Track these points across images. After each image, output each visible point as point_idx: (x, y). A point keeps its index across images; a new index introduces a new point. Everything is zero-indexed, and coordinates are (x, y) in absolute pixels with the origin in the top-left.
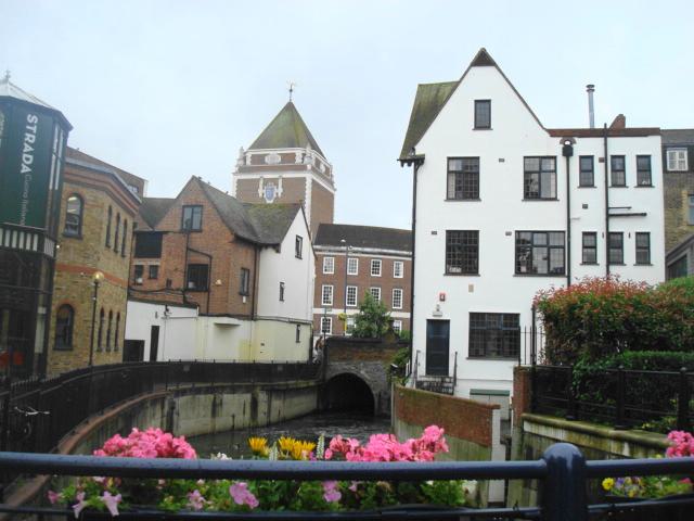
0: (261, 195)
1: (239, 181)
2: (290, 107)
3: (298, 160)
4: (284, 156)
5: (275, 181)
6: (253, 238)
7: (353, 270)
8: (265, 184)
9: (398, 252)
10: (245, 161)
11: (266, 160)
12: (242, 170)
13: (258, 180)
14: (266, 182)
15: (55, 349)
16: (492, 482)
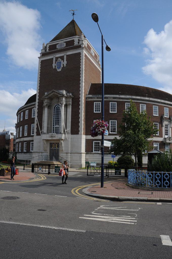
2: (73, 22)
3: (76, 43)
4: (68, 43)
5: (62, 58)
7: (113, 109)
8: (56, 61)
9: (142, 98)
10: (46, 50)
12: (43, 55)
15: (50, 143)
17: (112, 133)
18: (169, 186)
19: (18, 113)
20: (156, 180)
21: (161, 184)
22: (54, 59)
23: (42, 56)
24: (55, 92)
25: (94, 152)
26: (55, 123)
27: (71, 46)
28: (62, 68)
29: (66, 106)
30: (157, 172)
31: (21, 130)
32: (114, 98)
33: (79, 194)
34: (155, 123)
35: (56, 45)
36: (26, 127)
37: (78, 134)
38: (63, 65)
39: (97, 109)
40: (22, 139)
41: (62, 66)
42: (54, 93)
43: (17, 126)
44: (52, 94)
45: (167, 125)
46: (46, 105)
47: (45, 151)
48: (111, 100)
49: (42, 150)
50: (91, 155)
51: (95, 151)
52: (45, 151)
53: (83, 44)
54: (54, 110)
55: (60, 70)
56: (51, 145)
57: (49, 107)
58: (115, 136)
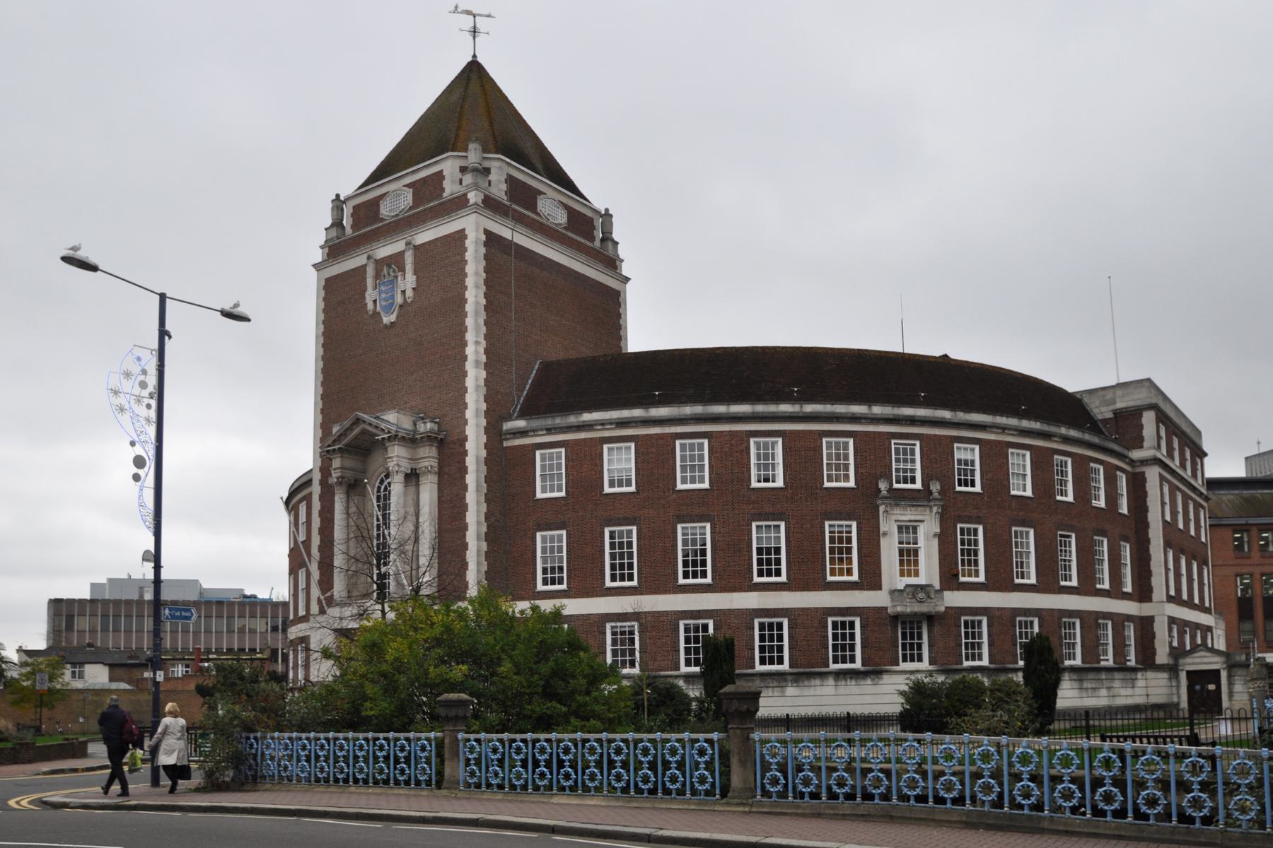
0: (370, 306)
5: (396, 261)
13: (402, 253)
17: (550, 587)
22: (370, 271)
27: (431, 201)
28: (401, 306)
35: (375, 203)
38: (404, 292)
42: (362, 426)
44: (356, 431)
45: (915, 529)
46: (339, 483)
48: (607, 434)
51: (763, 662)
55: (393, 318)
58: (557, 602)
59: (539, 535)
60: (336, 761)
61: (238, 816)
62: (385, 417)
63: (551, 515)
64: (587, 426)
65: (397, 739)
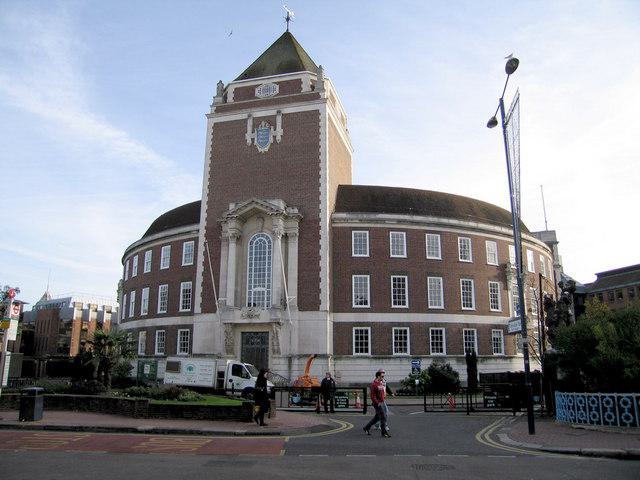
0: (249, 141)
1: (217, 126)
3: (306, 88)
5: (271, 121)
6: (499, 110)
10: (225, 98)
11: (257, 94)
12: (221, 108)
13: (245, 121)
14: (257, 122)
16: (465, 367)
18: (633, 425)
19: (127, 258)
20: (605, 410)
21: (616, 419)
23: (217, 111)
24: (257, 203)
25: (354, 354)
26: (255, 282)
29: (286, 237)
30: (621, 395)
31: (133, 299)
32: (400, 222)
33: (490, 440)
34: (465, 280)
36: (146, 292)
37: (318, 309)
38: (275, 137)
39: (361, 251)
40: (149, 323)
41: (271, 140)
43: (125, 288)
47: (229, 350)
48: (392, 226)
49: (219, 347)
50: (349, 362)
51: (357, 351)
52: (229, 350)
53: (324, 90)
54: (251, 248)
56: (247, 338)
57: (239, 239)
59: (353, 277)
60: (573, 407)
61: (14, 431)
62: (510, 211)
63: (361, 267)
64: (383, 221)
65: (589, 397)
